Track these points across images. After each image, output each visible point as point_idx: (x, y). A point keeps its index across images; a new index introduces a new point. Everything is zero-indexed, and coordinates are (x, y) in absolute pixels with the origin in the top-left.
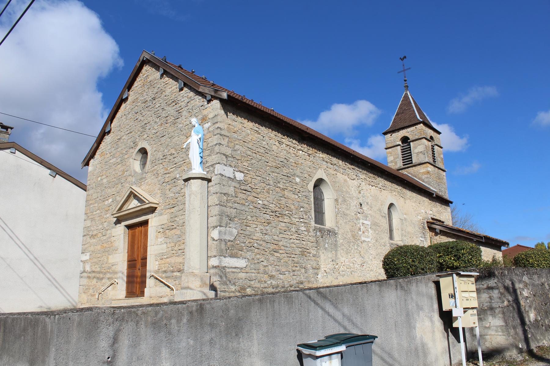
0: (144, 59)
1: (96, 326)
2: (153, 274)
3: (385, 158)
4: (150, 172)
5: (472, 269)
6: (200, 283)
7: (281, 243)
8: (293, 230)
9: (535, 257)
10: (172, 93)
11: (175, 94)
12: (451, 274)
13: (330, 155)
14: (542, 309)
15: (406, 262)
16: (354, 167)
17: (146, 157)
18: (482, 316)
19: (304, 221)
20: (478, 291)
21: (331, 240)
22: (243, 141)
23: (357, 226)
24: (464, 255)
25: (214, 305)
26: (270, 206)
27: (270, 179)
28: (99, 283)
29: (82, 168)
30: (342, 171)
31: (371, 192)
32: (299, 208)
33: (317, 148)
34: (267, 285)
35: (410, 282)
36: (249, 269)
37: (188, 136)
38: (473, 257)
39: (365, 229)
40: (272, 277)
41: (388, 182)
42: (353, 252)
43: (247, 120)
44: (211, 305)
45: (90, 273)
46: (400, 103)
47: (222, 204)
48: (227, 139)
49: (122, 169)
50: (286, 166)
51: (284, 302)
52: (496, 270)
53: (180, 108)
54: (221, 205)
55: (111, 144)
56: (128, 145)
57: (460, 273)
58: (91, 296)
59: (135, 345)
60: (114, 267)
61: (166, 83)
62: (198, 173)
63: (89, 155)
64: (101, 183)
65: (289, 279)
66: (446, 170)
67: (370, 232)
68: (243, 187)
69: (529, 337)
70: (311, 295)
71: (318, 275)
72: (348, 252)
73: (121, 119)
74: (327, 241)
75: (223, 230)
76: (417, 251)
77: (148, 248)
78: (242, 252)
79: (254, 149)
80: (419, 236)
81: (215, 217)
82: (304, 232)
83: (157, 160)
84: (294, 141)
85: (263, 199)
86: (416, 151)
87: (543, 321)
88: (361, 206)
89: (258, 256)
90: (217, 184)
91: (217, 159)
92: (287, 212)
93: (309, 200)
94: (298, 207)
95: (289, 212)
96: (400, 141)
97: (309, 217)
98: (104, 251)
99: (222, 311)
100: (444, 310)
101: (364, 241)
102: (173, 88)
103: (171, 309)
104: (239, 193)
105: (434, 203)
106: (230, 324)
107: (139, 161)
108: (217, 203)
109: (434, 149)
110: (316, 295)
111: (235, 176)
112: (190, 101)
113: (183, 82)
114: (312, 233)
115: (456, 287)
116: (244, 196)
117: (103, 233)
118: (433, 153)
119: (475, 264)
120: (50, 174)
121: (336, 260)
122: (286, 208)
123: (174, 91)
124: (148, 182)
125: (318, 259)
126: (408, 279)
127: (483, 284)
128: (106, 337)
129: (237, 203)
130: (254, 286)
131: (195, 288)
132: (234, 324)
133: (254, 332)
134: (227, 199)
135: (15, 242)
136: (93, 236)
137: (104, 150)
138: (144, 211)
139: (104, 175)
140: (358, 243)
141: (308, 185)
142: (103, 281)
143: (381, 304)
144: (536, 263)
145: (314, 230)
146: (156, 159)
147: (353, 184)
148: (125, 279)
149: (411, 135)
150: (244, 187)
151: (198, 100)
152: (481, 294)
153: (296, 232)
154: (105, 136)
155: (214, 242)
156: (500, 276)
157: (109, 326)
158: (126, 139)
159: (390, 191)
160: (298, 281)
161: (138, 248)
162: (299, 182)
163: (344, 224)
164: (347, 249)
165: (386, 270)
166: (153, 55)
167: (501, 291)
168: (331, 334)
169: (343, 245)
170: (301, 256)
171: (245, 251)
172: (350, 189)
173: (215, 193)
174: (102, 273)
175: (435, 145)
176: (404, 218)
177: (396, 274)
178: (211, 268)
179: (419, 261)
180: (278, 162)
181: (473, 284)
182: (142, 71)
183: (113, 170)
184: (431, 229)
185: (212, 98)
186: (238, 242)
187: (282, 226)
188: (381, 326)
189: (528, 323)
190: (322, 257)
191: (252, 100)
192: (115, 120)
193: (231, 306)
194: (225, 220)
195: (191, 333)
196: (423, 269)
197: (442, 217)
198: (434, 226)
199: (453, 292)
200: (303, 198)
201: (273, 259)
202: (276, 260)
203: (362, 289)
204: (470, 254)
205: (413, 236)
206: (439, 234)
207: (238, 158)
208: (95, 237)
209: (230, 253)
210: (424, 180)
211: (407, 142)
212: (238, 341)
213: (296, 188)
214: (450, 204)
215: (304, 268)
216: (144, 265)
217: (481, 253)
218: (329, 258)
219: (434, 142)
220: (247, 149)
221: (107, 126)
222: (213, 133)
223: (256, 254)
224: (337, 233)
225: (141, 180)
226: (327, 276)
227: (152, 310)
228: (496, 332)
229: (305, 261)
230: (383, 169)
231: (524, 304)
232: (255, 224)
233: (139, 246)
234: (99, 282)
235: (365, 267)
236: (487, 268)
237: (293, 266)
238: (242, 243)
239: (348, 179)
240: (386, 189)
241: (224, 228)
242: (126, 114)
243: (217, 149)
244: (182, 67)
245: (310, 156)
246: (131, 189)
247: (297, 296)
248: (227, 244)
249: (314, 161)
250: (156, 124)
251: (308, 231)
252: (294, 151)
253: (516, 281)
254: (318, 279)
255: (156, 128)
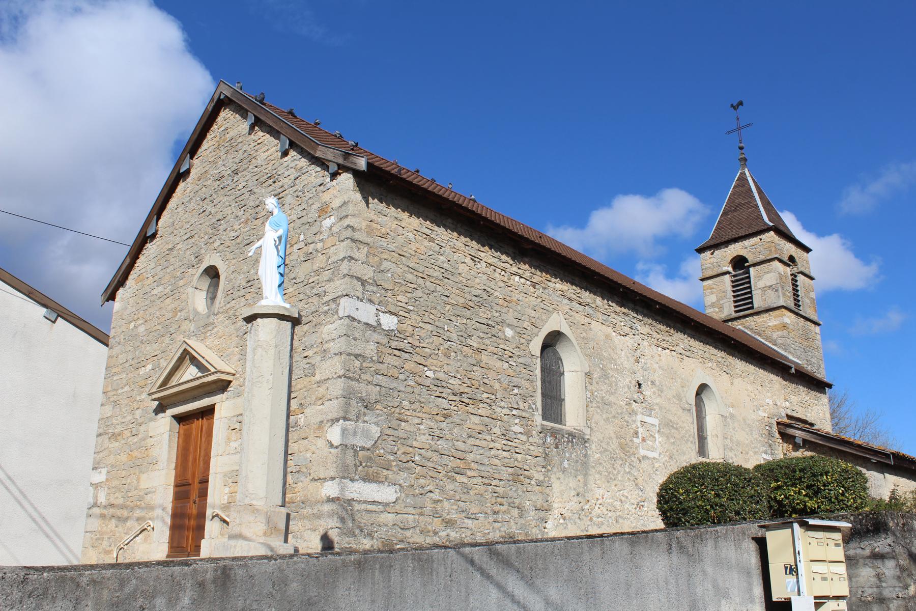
2: (217, 511)
5: (840, 516)
6: (265, 528)
8: (497, 430)
10: (268, 160)
11: (273, 162)
13: (576, 286)
15: (702, 496)
16: (626, 311)
17: (217, 285)
19: (521, 415)
20: (850, 561)
21: (576, 453)
22: (399, 255)
23: (629, 427)
25: (255, 571)
26: (450, 381)
27: (452, 329)
28: (120, 529)
30: (601, 318)
31: (660, 360)
33: (550, 271)
34: (438, 539)
35: (700, 537)
36: (403, 505)
37: (293, 243)
38: (846, 491)
40: (449, 523)
41: (697, 342)
45: (105, 507)
47: (351, 375)
48: (366, 248)
49: (173, 306)
51: (414, 570)
52: (892, 518)
54: (349, 378)
55: (156, 259)
56: (185, 261)
57: (808, 522)
58: (105, 552)
60: (148, 497)
61: (259, 141)
62: (272, 306)
64: (134, 333)
66: (821, 323)
67: (657, 438)
68: (394, 344)
70: (476, 558)
71: (546, 522)
72: (611, 478)
73: (176, 211)
74: (567, 455)
76: (726, 475)
77: (212, 459)
78: (389, 471)
79: (421, 269)
80: (761, 450)
81: (335, 401)
82: (519, 436)
83: (236, 290)
84: (504, 257)
85: (437, 369)
86: (761, 284)
89: (422, 481)
90: (342, 336)
92: (485, 395)
93: (531, 373)
94: (509, 385)
95: (490, 396)
96: (730, 265)
97: (530, 407)
98: (133, 465)
99: (271, 583)
100: (774, 599)
101: (646, 456)
102: (270, 152)
103: (157, 576)
110: (485, 558)
111: (378, 321)
112: (299, 176)
114: (536, 439)
115: (799, 552)
117: (134, 429)
118: (794, 289)
119: (851, 506)
120: (45, 317)
122: (484, 388)
123: (272, 157)
124: (218, 331)
125: (547, 491)
126: (697, 531)
127: (862, 546)
129: (382, 374)
130: (411, 540)
131: (254, 537)
134: (362, 366)
136: (115, 436)
137: (144, 270)
138: (207, 389)
140: (633, 461)
141: (531, 344)
142: (129, 524)
143: (634, 582)
145: (540, 433)
146: (233, 288)
148: (168, 520)
149: (750, 254)
150: (396, 343)
151: (315, 174)
154: (147, 243)
155: (332, 450)
156: (901, 531)
158: (183, 249)
159: (701, 360)
160: (504, 534)
161: (195, 459)
162: (512, 337)
163: (603, 422)
165: (664, 513)
166: (240, 92)
167: (902, 562)
169: (600, 464)
170: (511, 483)
171: (394, 469)
174: (126, 507)
175: (798, 273)
177: (681, 521)
179: (730, 496)
180: (469, 297)
181: (837, 545)
182: (217, 120)
183: (156, 309)
185: (339, 169)
186: (382, 451)
191: (432, 179)
192: (165, 213)
194: (356, 407)
198: (791, 431)
200: (518, 369)
202: (459, 489)
203: (590, 549)
204: (840, 484)
205: (747, 449)
207: (386, 286)
208: (119, 438)
210: (775, 342)
211: (743, 267)
213: (506, 348)
214: (827, 388)
216: (203, 494)
217: (866, 483)
218: (570, 488)
219: (798, 268)
224: (588, 439)
225: (205, 329)
226: (565, 525)
227: (114, 577)
229: (520, 493)
230: (685, 316)
232: (418, 417)
234: (120, 527)
235: (646, 509)
237: (496, 503)
238: (389, 453)
239: (614, 334)
240: (693, 355)
241: (354, 422)
242: (185, 201)
243: (344, 267)
245: (536, 287)
246: (185, 346)
247: (444, 559)
249: (544, 296)
250: (237, 220)
251: (528, 434)
252: (503, 275)
254: (546, 530)
255: (236, 227)
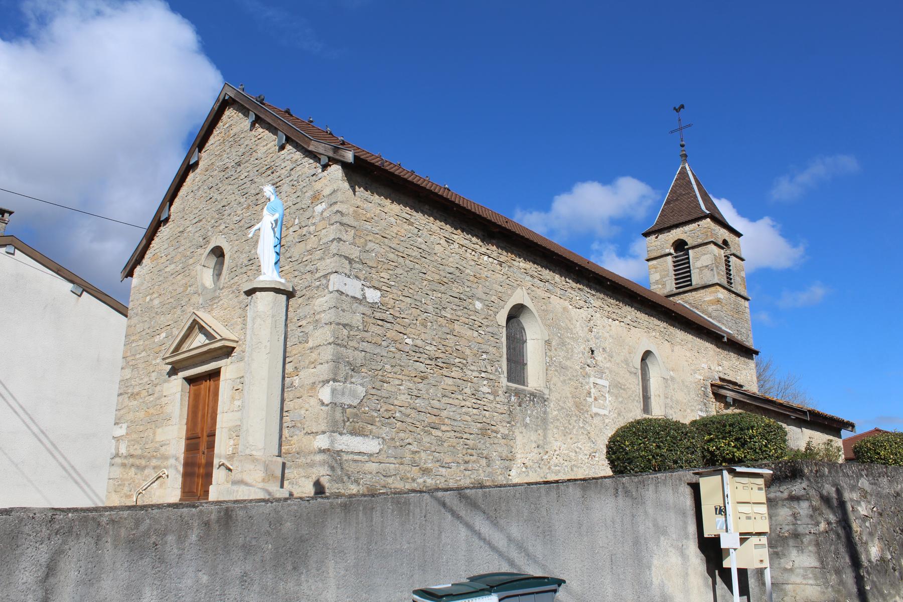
0: (226, 98)
1: (14, 544)
2: (223, 461)
3: (647, 279)
4: (227, 287)
5: (763, 464)
6: (263, 475)
7: (444, 414)
8: (468, 391)
9: (891, 446)
10: (267, 153)
12: (720, 471)
14: (895, 540)
15: (645, 448)
16: (581, 286)
17: (222, 263)
18: (779, 549)
19: (488, 377)
20: (771, 503)
21: (537, 410)
22: (382, 237)
24: (753, 439)
25: (253, 512)
26: (427, 348)
27: (428, 302)
28: (139, 476)
29: (121, 281)
30: (559, 293)
32: (479, 353)
33: (515, 252)
34: (416, 485)
36: (385, 456)
38: (769, 443)
39: (599, 394)
40: (426, 471)
41: (643, 315)
42: (577, 433)
43: (390, 200)
44: (247, 512)
46: (672, 184)
47: (340, 342)
49: (184, 282)
50: (458, 281)
53: (279, 179)
54: (338, 345)
56: (194, 242)
57: (736, 470)
59: (90, 581)
61: (259, 137)
63: (134, 259)
65: (458, 475)
66: (750, 298)
67: (607, 398)
68: (378, 315)
69: (867, 590)
70: (447, 501)
71: (510, 470)
72: (567, 432)
74: (529, 412)
75: (339, 388)
76: (666, 429)
78: (373, 426)
79: (401, 249)
80: (697, 408)
81: (326, 365)
82: (487, 396)
83: (239, 268)
84: (474, 239)
85: (415, 337)
86: (699, 264)
87: (896, 562)
88: (592, 354)
89: (402, 435)
90: (332, 308)
91: (333, 265)
92: (457, 360)
93: (498, 341)
95: (461, 360)
97: (496, 370)
100: (706, 535)
102: (269, 146)
103: (168, 517)
104: (371, 325)
105: (724, 353)
106: (284, 548)
107: (212, 270)
108: (331, 340)
109: (729, 262)
111: (364, 295)
112: (295, 167)
113: (285, 135)
114: (502, 398)
115: (727, 495)
116: (380, 331)
117: (150, 390)
118: (727, 269)
119: (772, 455)
120: (71, 291)
121: (545, 446)
123: (270, 151)
124: (223, 304)
125: (511, 443)
127: (781, 490)
128: (33, 565)
129: (367, 341)
131: (254, 483)
132: (290, 549)
133: (331, 564)
134: (349, 334)
135: (8, 403)
136: (133, 396)
137: (158, 250)
138: (214, 354)
139: (155, 292)
140: (586, 418)
141: (498, 315)
142: (146, 472)
144: (892, 457)
145: (506, 393)
146: (237, 266)
147: (579, 315)
148: (181, 469)
149: (689, 238)
151: (308, 166)
152: (778, 508)
153: (473, 394)
154: (161, 226)
155: (323, 408)
156: (814, 476)
157: (41, 544)
158: (193, 232)
160: (473, 480)
161: (203, 416)
162: (481, 309)
163: (560, 383)
164: (565, 428)
165: (612, 463)
167: (814, 503)
168: (484, 573)
171: (378, 424)
172: (572, 324)
173: (328, 324)
175: (731, 255)
176: (671, 376)
177: (627, 469)
178: (317, 452)
181: (760, 489)
182: (222, 118)
184: (719, 397)
185: (329, 161)
186: (367, 409)
187: (447, 384)
188: (582, 561)
189: (865, 563)
190: (520, 440)
192: (176, 200)
193: (287, 515)
194: (344, 370)
195: (204, 562)
196: (675, 462)
197: (739, 378)
198: (723, 392)
199: (723, 503)
200: (486, 337)
201: (429, 440)
203: (547, 493)
204: (763, 436)
206: (731, 406)
207: (371, 264)
208: (137, 397)
209: (350, 428)
210: (710, 314)
211: (683, 250)
212: (297, 580)
213: (476, 319)
215: (486, 458)
216: (211, 446)
217: (786, 436)
218: (531, 441)
220: (388, 249)
221: (165, 209)
222: (329, 221)
223: (399, 431)
224: (547, 398)
225: (212, 301)
228: (805, 579)
229: (488, 445)
230: (633, 291)
231: (859, 529)
233: (205, 414)
234: (139, 474)
235: (597, 459)
236: (789, 462)
237: (466, 454)
238: (373, 410)
239: (570, 307)
240: (639, 326)
241: (342, 383)
242: (194, 189)
243: (334, 248)
244: (291, 113)
248: (346, 413)
249: (509, 273)
251: (495, 394)
252: (474, 255)
253: (845, 486)
254: (510, 477)
255: (239, 212)
